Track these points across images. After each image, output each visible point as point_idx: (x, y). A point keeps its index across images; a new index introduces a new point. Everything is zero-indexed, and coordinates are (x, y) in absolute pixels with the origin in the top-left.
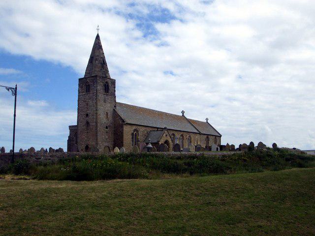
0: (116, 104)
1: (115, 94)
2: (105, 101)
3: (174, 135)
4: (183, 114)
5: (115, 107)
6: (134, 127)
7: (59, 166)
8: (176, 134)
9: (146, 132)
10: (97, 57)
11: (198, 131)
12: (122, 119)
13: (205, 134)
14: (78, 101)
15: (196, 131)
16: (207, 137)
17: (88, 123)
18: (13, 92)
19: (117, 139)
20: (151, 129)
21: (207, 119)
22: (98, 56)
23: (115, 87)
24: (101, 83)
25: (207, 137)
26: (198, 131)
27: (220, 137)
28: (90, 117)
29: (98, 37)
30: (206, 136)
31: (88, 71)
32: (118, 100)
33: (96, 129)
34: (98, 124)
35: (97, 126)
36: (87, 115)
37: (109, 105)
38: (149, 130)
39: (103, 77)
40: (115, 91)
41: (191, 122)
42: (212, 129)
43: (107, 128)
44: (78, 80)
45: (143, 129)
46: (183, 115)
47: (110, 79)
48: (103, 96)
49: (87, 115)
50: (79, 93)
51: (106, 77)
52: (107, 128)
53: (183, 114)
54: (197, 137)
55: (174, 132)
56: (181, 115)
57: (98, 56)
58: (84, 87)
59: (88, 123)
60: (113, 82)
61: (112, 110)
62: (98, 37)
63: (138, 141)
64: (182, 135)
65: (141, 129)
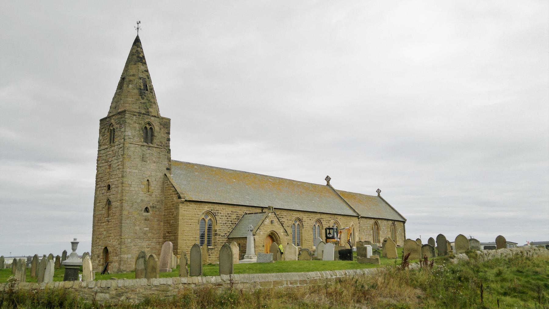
0: (170, 165)
1: (169, 146)
2: (143, 159)
4: (328, 182)
6: (206, 208)
7: (276, 279)
8: (304, 217)
9: (234, 216)
10: (132, 78)
11: (354, 211)
12: (177, 193)
13: (388, 220)
14: (98, 160)
15: (351, 213)
16: (376, 223)
19: (168, 233)
20: (246, 210)
22: (133, 75)
24: (137, 125)
25: (376, 223)
26: (354, 211)
27: (404, 222)
28: (113, 190)
29: (137, 42)
30: (373, 221)
31: (114, 105)
33: (121, 215)
34: (125, 205)
35: (122, 206)
37: (153, 166)
38: (241, 211)
39: (140, 113)
40: (169, 140)
41: (341, 196)
42: (389, 207)
43: (147, 210)
44: (99, 122)
45: (229, 209)
47: (158, 117)
48: (138, 149)
49: (109, 187)
50: (100, 146)
51: (148, 113)
52: (147, 210)
53: (328, 182)
54: (353, 222)
55: (300, 215)
57: (133, 75)
58: (107, 134)
59: (109, 202)
60: (166, 124)
61: (160, 175)
62: (137, 42)
63: (216, 234)
65: (224, 211)
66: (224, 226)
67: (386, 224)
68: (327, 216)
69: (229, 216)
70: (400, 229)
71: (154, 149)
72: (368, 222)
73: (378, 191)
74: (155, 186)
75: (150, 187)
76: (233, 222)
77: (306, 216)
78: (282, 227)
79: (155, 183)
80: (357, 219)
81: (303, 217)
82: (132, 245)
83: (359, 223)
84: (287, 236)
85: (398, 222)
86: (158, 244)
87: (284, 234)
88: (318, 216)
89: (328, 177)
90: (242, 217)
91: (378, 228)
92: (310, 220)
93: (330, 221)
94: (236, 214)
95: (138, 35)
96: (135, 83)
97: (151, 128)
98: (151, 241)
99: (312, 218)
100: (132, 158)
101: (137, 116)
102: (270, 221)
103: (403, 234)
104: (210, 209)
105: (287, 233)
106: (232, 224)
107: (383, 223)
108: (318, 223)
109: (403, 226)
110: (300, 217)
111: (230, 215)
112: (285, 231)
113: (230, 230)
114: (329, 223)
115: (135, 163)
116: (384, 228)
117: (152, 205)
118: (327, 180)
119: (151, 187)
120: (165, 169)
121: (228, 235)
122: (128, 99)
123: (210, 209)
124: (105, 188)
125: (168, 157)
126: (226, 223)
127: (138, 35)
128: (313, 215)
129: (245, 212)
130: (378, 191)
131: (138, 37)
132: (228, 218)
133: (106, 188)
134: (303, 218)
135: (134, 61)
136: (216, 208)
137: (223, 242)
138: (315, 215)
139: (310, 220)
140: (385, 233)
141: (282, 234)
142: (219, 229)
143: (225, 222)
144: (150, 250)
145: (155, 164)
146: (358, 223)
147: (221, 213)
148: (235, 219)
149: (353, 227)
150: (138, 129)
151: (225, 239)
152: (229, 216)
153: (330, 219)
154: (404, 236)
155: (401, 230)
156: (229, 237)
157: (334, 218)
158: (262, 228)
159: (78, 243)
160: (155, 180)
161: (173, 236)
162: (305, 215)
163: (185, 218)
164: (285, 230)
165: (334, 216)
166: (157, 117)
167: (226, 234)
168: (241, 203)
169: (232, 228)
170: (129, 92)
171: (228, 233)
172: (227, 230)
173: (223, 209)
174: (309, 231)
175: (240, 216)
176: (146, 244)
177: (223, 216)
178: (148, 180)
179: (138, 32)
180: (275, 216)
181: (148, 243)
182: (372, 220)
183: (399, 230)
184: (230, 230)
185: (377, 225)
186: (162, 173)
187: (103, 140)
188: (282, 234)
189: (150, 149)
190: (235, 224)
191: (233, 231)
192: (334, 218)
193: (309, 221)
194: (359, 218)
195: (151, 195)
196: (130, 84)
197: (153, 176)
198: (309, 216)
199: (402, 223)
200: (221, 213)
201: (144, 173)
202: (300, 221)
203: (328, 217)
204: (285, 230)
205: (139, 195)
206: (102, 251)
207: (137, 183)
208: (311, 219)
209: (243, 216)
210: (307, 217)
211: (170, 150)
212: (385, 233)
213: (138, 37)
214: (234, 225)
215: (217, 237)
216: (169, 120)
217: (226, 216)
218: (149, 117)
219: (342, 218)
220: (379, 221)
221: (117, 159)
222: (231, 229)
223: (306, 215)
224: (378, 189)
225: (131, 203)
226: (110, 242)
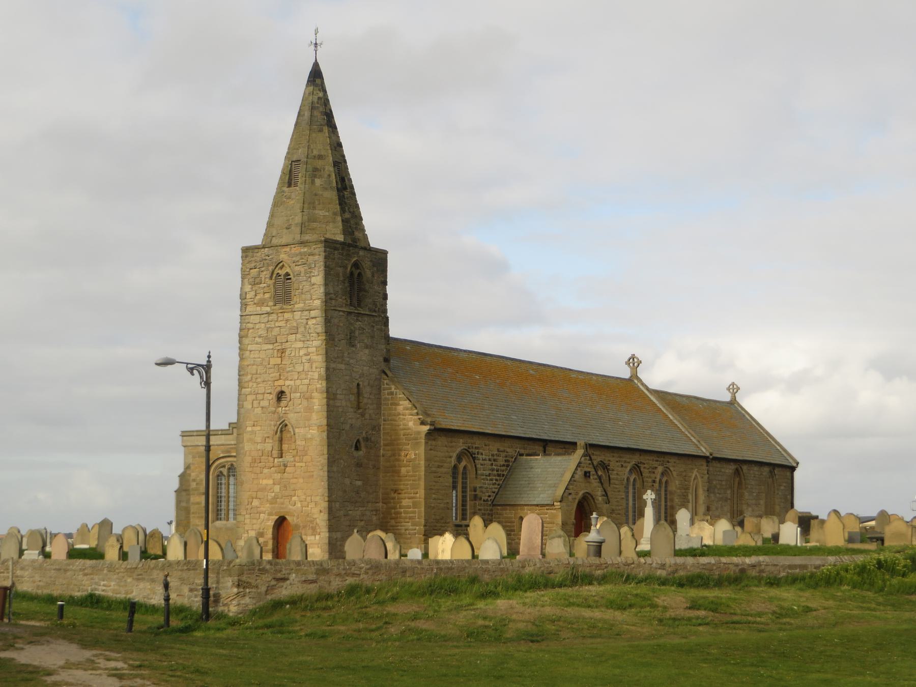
3: (605, 466)
5: (386, 360)
6: (460, 444)
8: (613, 460)
9: (501, 460)
16: (737, 472)
17: (283, 428)
18: (201, 377)
21: (633, 362)
23: (385, 283)
27: (793, 469)
29: (316, 76)
30: (731, 468)
32: (396, 330)
36: (280, 395)
37: (364, 355)
45: (494, 446)
46: (635, 376)
47: (368, 249)
50: (244, 306)
56: (625, 373)
59: (283, 428)
62: (316, 76)
64: (636, 468)
66: (487, 480)
67: (757, 473)
68: (651, 458)
69: (495, 460)
70: (784, 484)
71: (366, 318)
72: (723, 470)
73: (631, 360)
74: (369, 397)
75: (361, 398)
76: (499, 473)
77: (614, 458)
78: (600, 485)
79: (368, 389)
80: (705, 464)
81: (609, 461)
82: (342, 513)
83: (708, 473)
84: (606, 503)
85: (780, 469)
86: (374, 513)
87: (603, 500)
88: (635, 459)
89: (633, 357)
90: (514, 462)
91: (740, 483)
92: (622, 466)
93: (656, 468)
94: (504, 455)
95: (316, 60)
96: (326, 176)
97: (359, 274)
98: (365, 508)
99: (625, 462)
100: (336, 340)
101: (340, 251)
102: (583, 472)
103: (789, 497)
104: (467, 445)
105: (607, 497)
106: (499, 475)
107: (752, 472)
108: (633, 474)
109: (790, 478)
110: (604, 459)
111: (495, 457)
112: (604, 493)
113: (496, 488)
114: (654, 473)
115: (341, 350)
116: (753, 483)
117: (366, 436)
118: (731, 390)
119: (363, 397)
120: (381, 359)
121: (493, 498)
122: (317, 212)
123: (467, 445)
124: (270, 396)
125: (385, 334)
126: (489, 475)
127: (316, 60)
128: (627, 457)
129: (518, 450)
130: (731, 387)
131: (316, 66)
132: (492, 465)
133: (273, 397)
134: (611, 463)
135: (319, 123)
136: (475, 443)
137: (485, 512)
138: (631, 456)
139: (622, 466)
140: (755, 494)
141: (600, 499)
142: (479, 485)
143: (487, 472)
144: (365, 526)
145: (367, 351)
146: (706, 472)
147: (482, 454)
148: (504, 465)
149: (696, 481)
150: (341, 278)
151: (488, 508)
152: (495, 460)
153: (655, 464)
154: (790, 500)
155: (785, 486)
156: (494, 503)
157: (663, 461)
158: (571, 487)
159: (486, 526)
160: (369, 384)
161: (409, 499)
162: (613, 456)
163: (433, 465)
164: (605, 491)
165: (664, 457)
166: (368, 250)
167: (489, 496)
168: (548, 436)
169: (498, 485)
170: (316, 195)
171: (493, 494)
172: (492, 488)
173: (486, 445)
174: (619, 491)
175: (510, 459)
176: (359, 513)
177: (485, 460)
178: (358, 385)
179: (316, 58)
180: (590, 462)
181: (361, 511)
182: (732, 464)
183: (782, 488)
184: (496, 488)
185: (740, 478)
186: (378, 368)
187: (253, 293)
188: (600, 499)
189: (360, 318)
190: (503, 475)
191: (501, 490)
192: (663, 461)
193: (620, 469)
194: (708, 462)
195: (363, 415)
196: (315, 176)
197: (365, 375)
198: (621, 457)
199: (788, 469)
200: (482, 454)
201: (353, 371)
202: (604, 469)
203: (653, 460)
204: (605, 491)
205: (348, 414)
206: (273, 524)
207: (344, 392)
208: (624, 465)
209: (515, 459)
210: (617, 459)
211: (387, 318)
212: (755, 494)
213: (316, 66)
214: (501, 478)
215: (477, 502)
216: (385, 253)
217: (490, 460)
218: (357, 250)
219: (678, 461)
220: (745, 467)
221: (302, 339)
222: (496, 486)
223: (615, 455)
224: (733, 384)
225: (337, 430)
226: (294, 508)
